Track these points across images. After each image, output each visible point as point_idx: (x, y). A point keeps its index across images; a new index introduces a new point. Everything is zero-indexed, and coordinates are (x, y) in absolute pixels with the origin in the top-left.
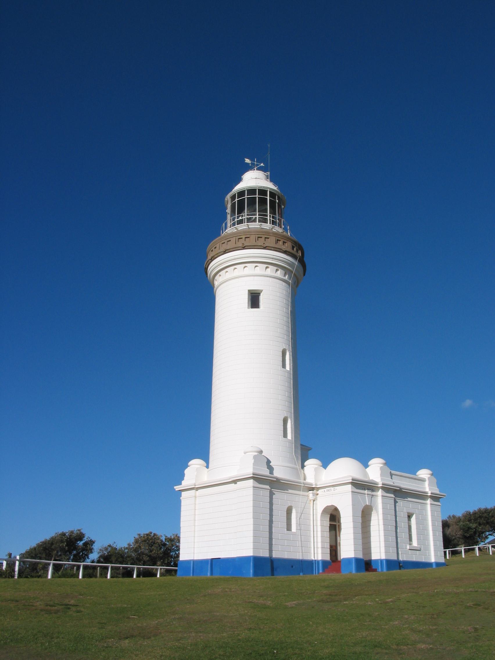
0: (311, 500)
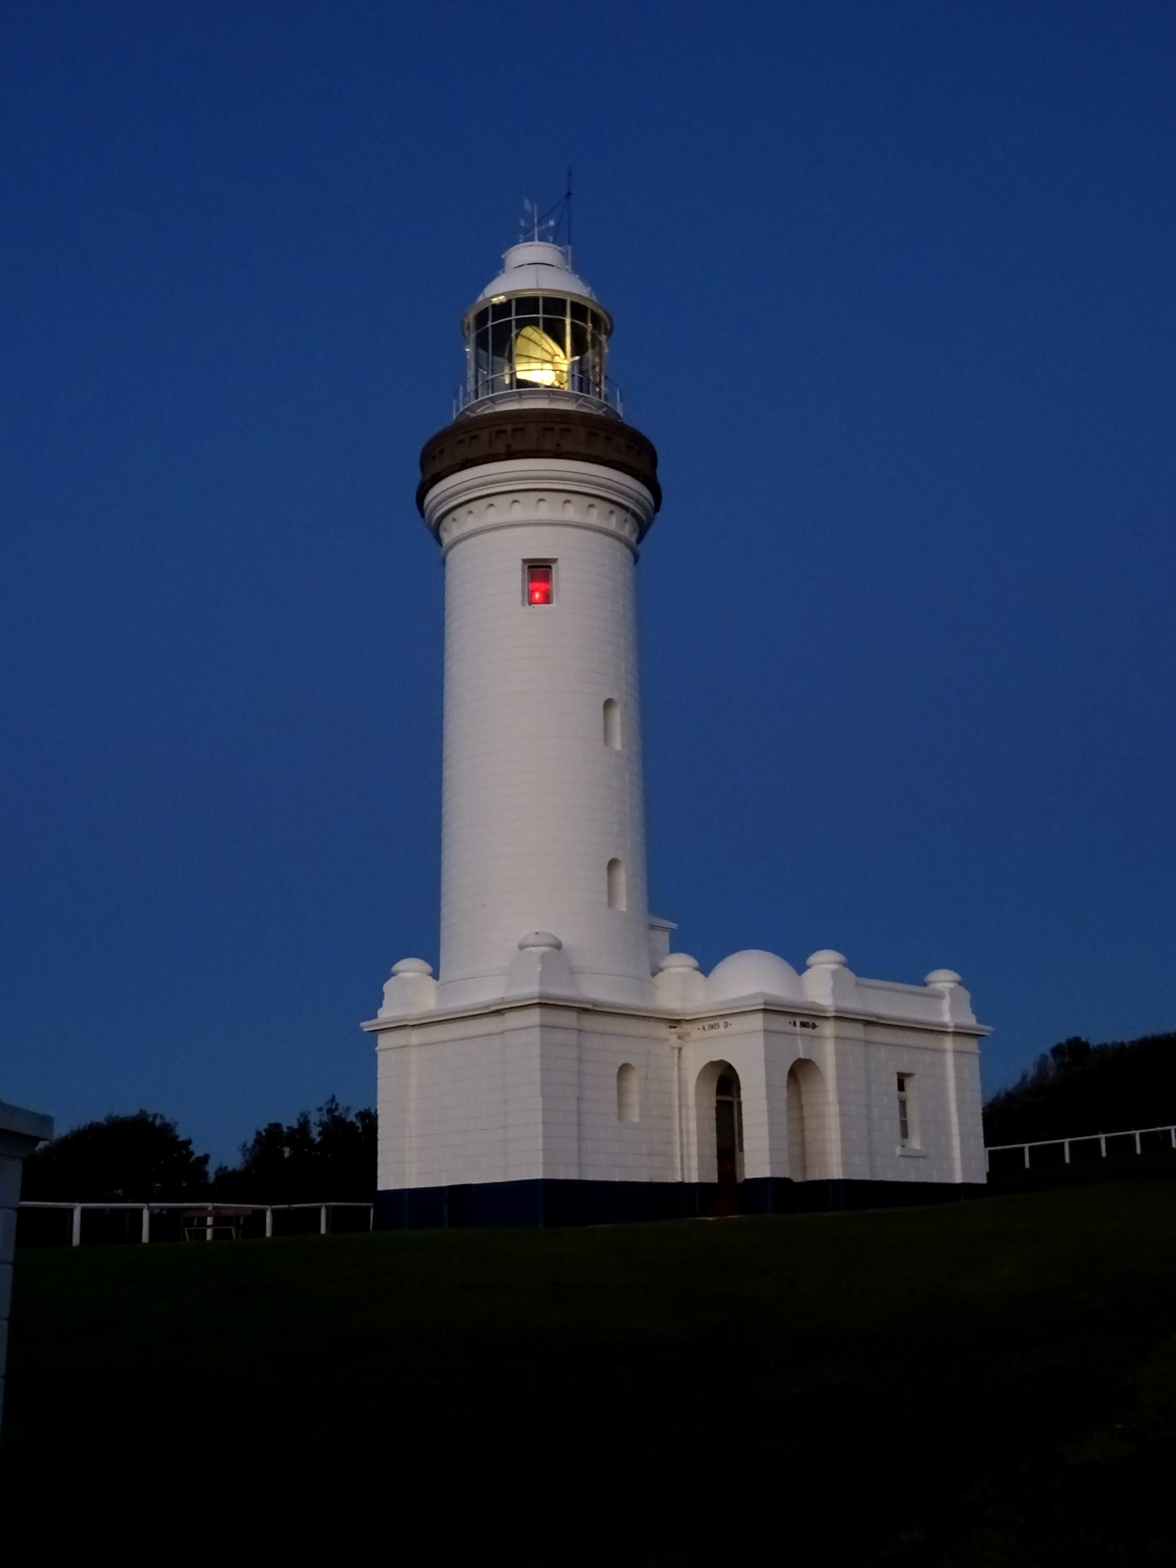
0: (673, 1048)
